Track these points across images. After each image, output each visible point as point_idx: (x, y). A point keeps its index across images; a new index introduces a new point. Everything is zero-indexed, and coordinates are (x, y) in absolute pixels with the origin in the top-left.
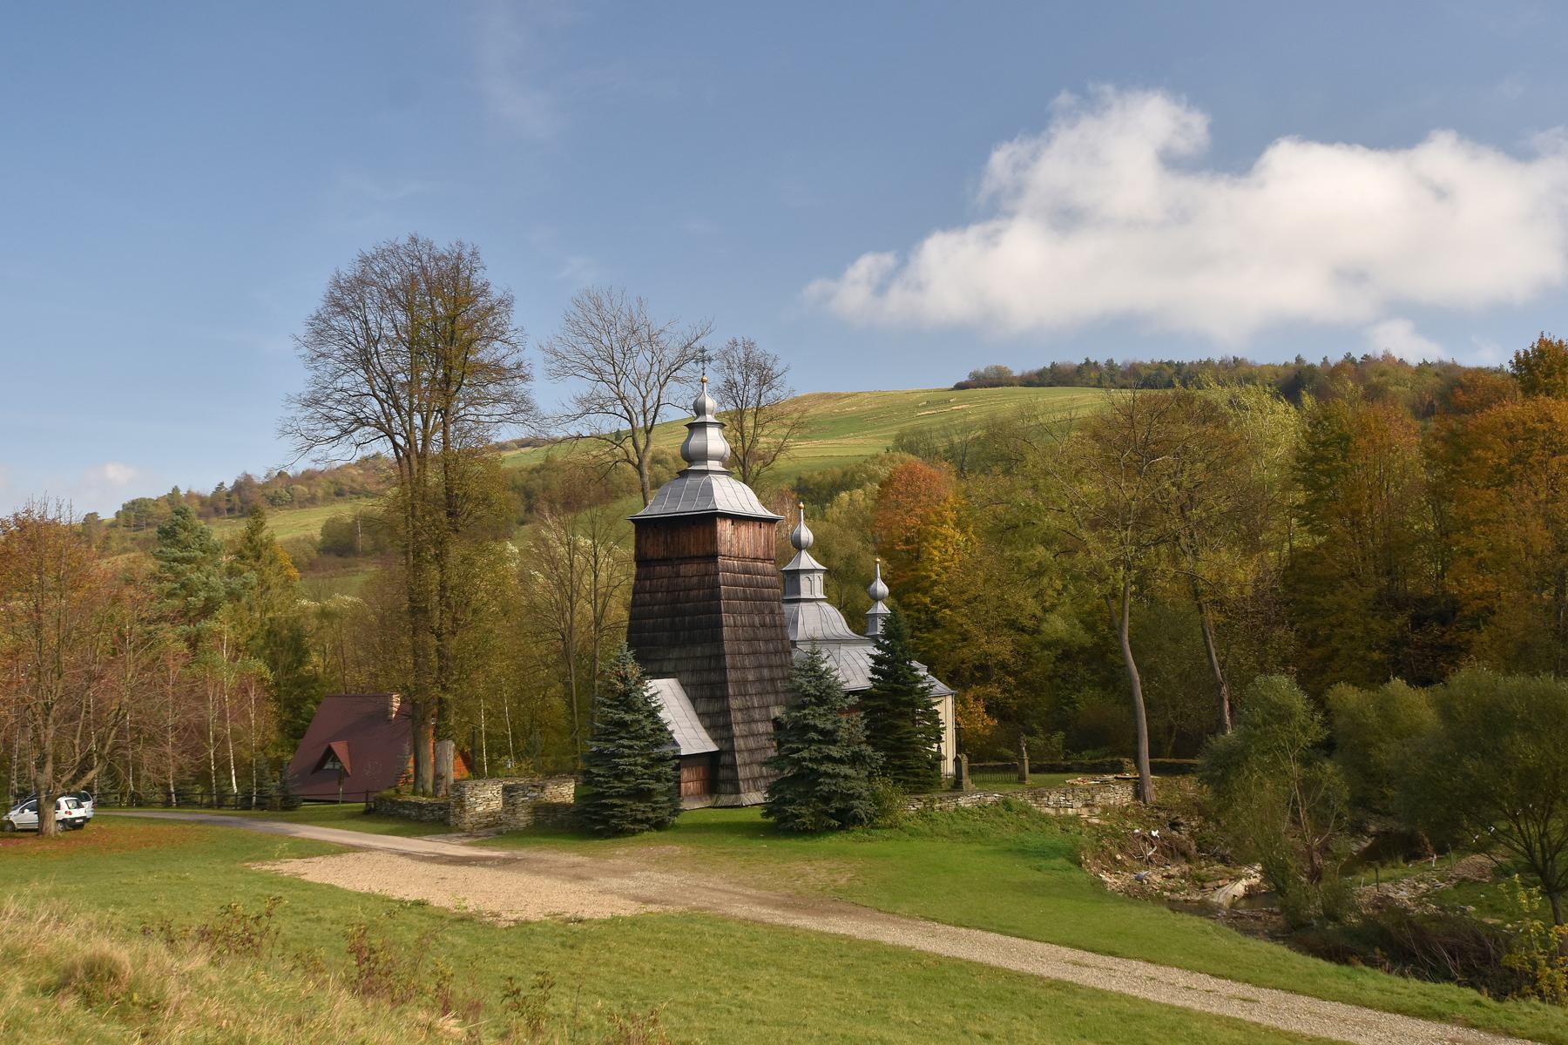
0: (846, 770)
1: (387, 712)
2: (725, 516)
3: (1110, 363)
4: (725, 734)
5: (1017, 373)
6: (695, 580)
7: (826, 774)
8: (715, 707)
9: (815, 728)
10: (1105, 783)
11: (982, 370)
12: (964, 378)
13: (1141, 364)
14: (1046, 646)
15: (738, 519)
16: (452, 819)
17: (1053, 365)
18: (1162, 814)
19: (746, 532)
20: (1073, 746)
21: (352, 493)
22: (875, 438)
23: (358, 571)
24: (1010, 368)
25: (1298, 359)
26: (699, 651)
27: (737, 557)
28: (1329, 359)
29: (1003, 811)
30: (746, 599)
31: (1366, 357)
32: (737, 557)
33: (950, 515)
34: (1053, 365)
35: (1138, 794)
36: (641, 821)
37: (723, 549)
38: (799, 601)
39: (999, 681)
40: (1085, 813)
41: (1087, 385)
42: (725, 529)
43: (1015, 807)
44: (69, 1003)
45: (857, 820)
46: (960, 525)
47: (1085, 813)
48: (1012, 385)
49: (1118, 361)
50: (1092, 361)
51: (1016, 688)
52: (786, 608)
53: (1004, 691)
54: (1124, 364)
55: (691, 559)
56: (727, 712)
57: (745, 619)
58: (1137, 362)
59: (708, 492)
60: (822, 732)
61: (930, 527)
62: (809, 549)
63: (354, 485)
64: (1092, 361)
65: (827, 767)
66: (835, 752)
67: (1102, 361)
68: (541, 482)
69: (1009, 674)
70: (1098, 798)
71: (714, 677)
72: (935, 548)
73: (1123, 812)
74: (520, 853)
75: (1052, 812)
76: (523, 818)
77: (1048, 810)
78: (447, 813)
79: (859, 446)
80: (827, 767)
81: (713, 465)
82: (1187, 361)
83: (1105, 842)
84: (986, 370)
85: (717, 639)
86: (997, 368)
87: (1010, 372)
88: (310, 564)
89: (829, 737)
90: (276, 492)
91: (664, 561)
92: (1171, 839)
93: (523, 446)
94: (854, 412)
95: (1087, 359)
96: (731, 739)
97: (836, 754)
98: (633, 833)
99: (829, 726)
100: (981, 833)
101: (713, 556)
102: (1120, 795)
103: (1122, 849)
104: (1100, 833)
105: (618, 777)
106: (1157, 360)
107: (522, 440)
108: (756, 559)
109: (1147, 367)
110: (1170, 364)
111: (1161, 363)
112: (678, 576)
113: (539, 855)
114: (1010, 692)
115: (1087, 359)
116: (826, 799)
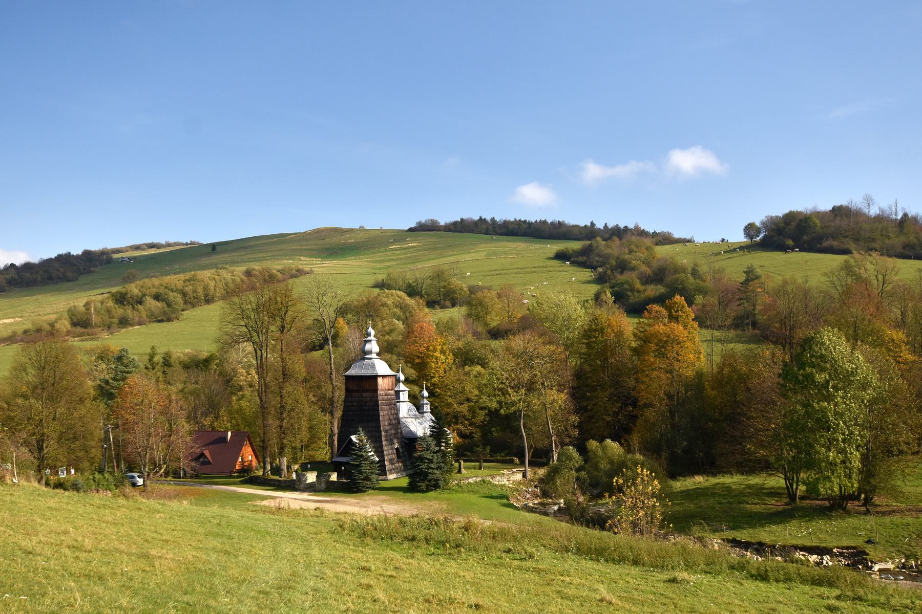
0: (436, 471)
1: (225, 438)
2: (380, 376)
3: (493, 219)
4: (381, 454)
5: (442, 223)
6: (369, 399)
7: (430, 473)
8: (377, 445)
9: (426, 458)
10: (513, 473)
11: (423, 221)
12: (413, 225)
13: (509, 221)
14: (482, 409)
15: (384, 376)
16: (296, 486)
17: (462, 219)
18: (532, 483)
19: (386, 380)
20: (494, 451)
21: (58, 278)
22: (367, 261)
23: (98, 338)
24: (439, 221)
25: (592, 224)
26: (370, 424)
27: (383, 390)
28: (608, 225)
29: (482, 483)
30: (386, 405)
31: (626, 227)
32: (383, 390)
33: (439, 347)
34: (462, 219)
35: (524, 476)
36: (368, 488)
37: (379, 388)
38: (400, 402)
39: (462, 423)
40: (507, 483)
41: (480, 233)
42: (380, 380)
43: (487, 482)
44: (463, 530)
45: (439, 487)
46: (443, 352)
47: (507, 483)
48: (440, 230)
49: (497, 219)
50: (483, 218)
51: (469, 426)
52: (398, 404)
53: (464, 426)
54: (500, 221)
55: (367, 391)
56: (382, 446)
57: (386, 413)
58: (507, 220)
59: (373, 366)
60: (428, 459)
61: (430, 353)
62: (426, 398)
63: (60, 274)
64: (483, 218)
65: (430, 471)
66: (433, 466)
67: (488, 218)
68: (191, 287)
69: (467, 420)
70: (511, 478)
71: (377, 434)
72: (432, 362)
73: (519, 483)
74: (334, 498)
75: (497, 483)
76: (323, 486)
77: (495, 483)
78: (295, 484)
79: (360, 266)
80: (430, 471)
81: (374, 356)
82: (533, 220)
83: (514, 493)
84: (425, 221)
85: (379, 421)
86: (431, 220)
87: (439, 223)
88: (67, 332)
89: (431, 461)
90: (12, 277)
91: (357, 391)
92: (534, 491)
93: (151, 248)
94: (352, 243)
95: (481, 217)
96: (383, 456)
97: (433, 467)
98: (365, 491)
99: (431, 458)
100: (478, 491)
101: (376, 390)
102: (518, 477)
103: (519, 495)
104: (513, 490)
105: (361, 474)
106: (518, 219)
107: (150, 244)
108: (389, 390)
109: (512, 223)
110: (525, 222)
111: (520, 220)
112: (362, 397)
113: (339, 499)
114: (466, 427)
115: (481, 217)
116: (430, 481)
